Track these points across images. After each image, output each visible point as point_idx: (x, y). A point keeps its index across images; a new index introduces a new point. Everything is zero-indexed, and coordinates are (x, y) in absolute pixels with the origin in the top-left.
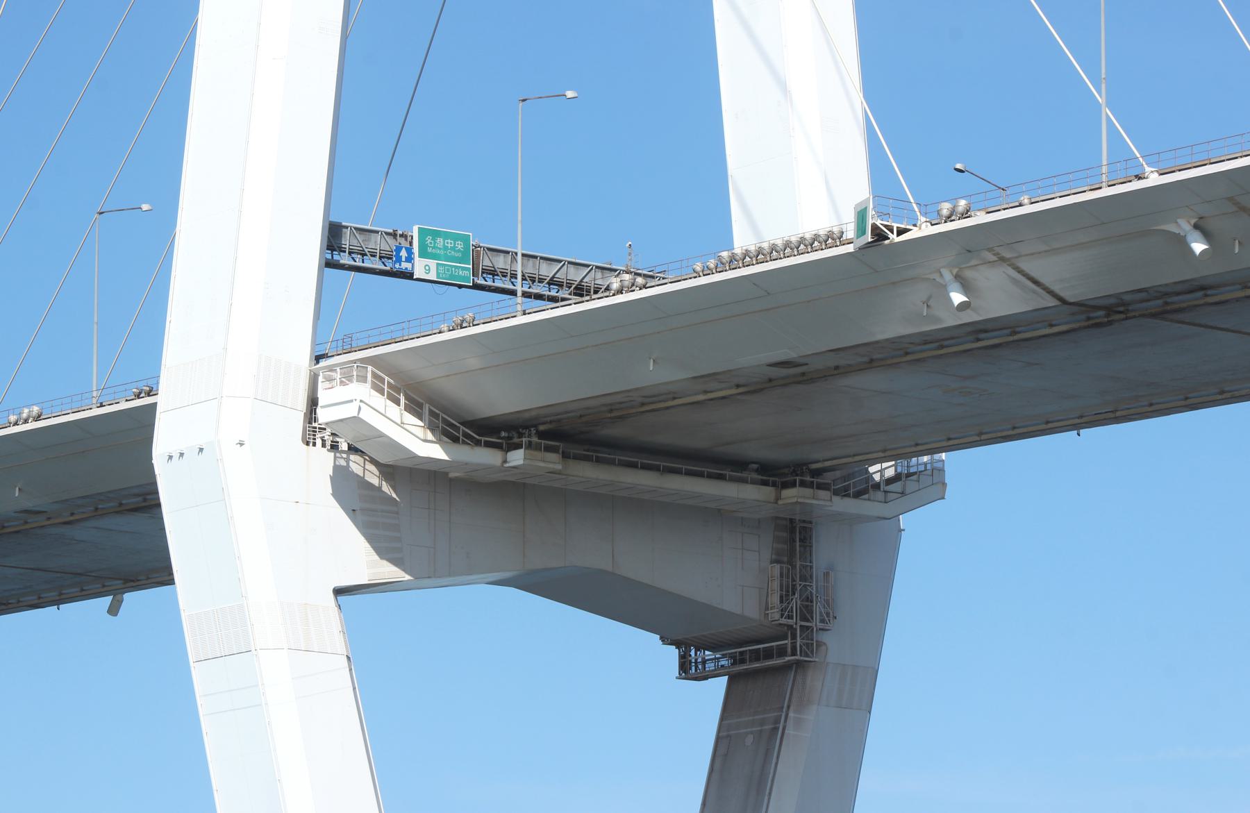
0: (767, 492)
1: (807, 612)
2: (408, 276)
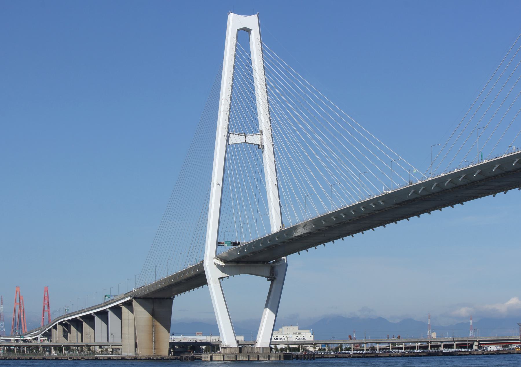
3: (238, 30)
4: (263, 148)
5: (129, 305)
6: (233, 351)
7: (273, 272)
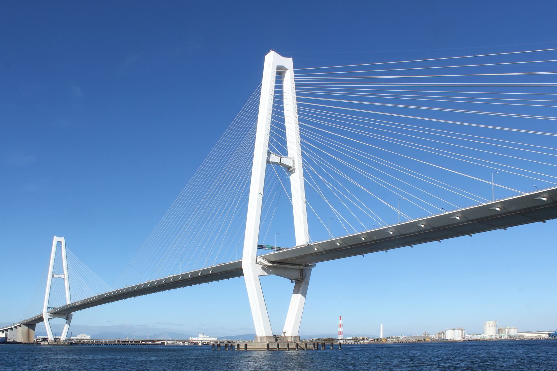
0: (299, 267)
1: (302, 277)
2: (265, 249)
3: (57, 242)
4: (65, 279)
5: (20, 326)
6: (52, 341)
7: (303, 274)
